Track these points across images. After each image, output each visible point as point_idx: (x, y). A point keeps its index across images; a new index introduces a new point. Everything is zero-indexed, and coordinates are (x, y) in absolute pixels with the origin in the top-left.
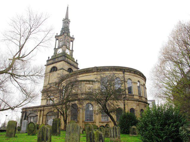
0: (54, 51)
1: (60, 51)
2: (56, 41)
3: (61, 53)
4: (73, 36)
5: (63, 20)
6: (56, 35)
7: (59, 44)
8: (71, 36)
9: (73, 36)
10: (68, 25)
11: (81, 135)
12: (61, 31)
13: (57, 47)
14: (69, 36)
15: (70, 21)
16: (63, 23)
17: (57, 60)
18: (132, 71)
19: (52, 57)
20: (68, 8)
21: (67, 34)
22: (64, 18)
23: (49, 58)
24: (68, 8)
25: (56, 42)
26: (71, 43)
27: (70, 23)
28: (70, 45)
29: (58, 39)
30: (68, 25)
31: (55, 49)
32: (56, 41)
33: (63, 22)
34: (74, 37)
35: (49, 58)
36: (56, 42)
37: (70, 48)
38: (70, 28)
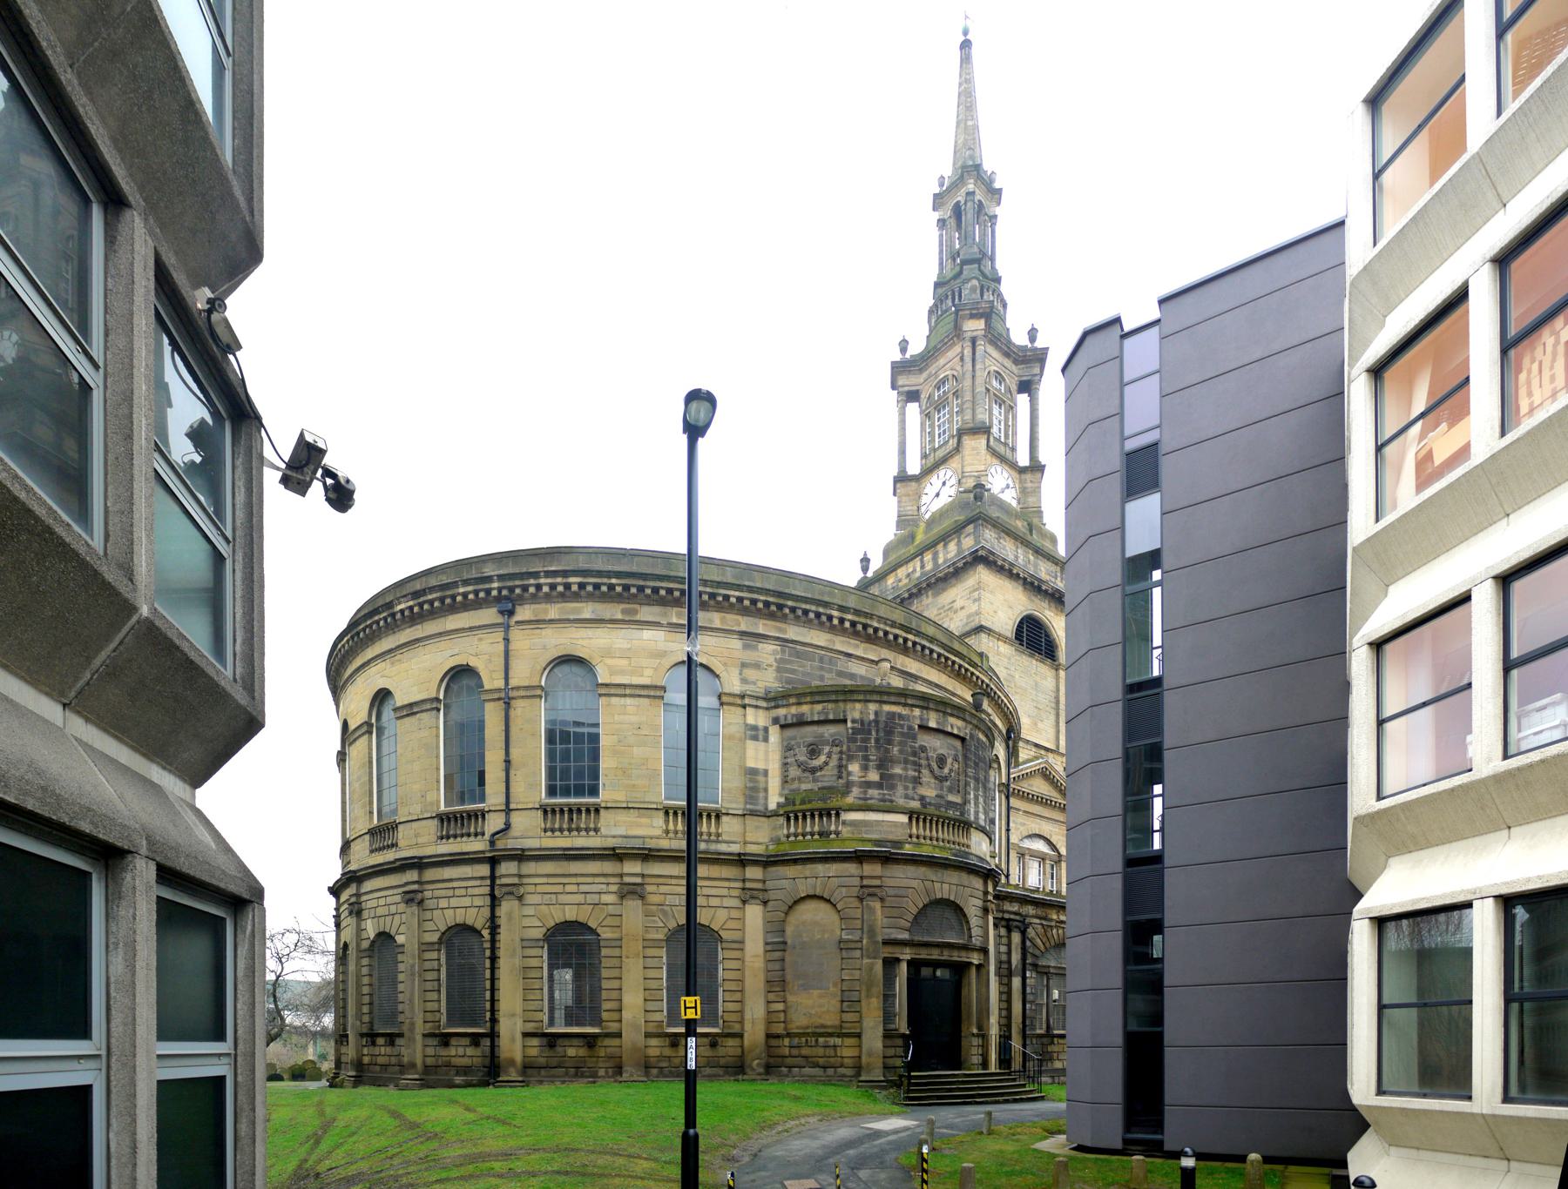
0: (1008, 325)
1: (940, 493)
2: (902, 414)
3: (956, 505)
4: (1033, 333)
5: (938, 201)
6: (898, 357)
7: (927, 433)
8: (1019, 338)
9: (1033, 333)
10: (983, 235)
11: (970, 726)
12: (931, 312)
13: (914, 468)
14: (999, 339)
15: (996, 194)
16: (942, 223)
17: (210, 363)
18: (536, 575)
19: (887, 552)
20: (966, 45)
21: (988, 326)
22: (948, 171)
23: (865, 562)
24: (966, 45)
25: (902, 422)
26: (1023, 400)
27: (998, 211)
28: (1011, 429)
29: (913, 396)
30: (983, 235)
31: (902, 479)
32: (902, 414)
33: (936, 215)
34: (1039, 344)
35: (865, 562)
36: (902, 422)
37: (1013, 449)
38: (1004, 264)
